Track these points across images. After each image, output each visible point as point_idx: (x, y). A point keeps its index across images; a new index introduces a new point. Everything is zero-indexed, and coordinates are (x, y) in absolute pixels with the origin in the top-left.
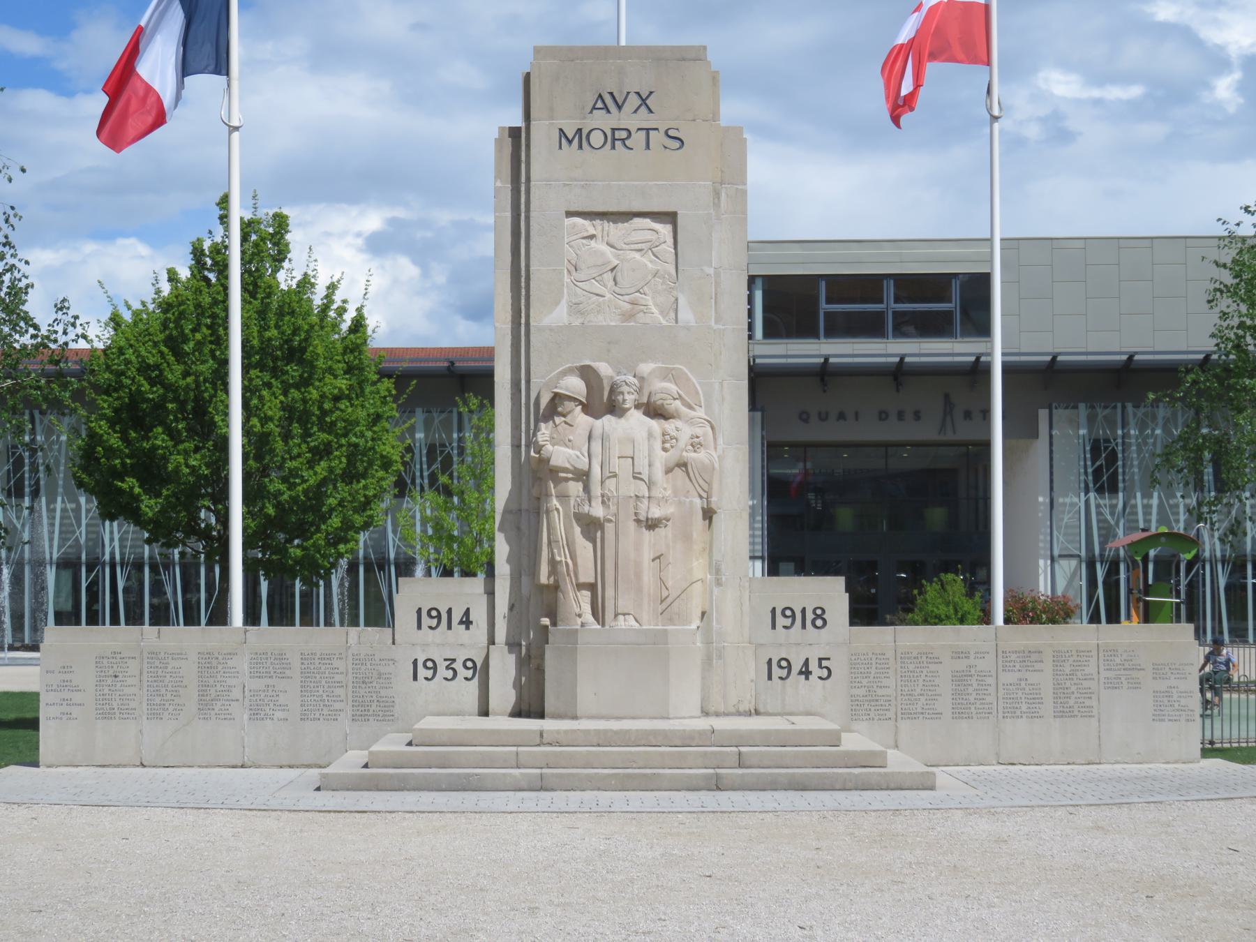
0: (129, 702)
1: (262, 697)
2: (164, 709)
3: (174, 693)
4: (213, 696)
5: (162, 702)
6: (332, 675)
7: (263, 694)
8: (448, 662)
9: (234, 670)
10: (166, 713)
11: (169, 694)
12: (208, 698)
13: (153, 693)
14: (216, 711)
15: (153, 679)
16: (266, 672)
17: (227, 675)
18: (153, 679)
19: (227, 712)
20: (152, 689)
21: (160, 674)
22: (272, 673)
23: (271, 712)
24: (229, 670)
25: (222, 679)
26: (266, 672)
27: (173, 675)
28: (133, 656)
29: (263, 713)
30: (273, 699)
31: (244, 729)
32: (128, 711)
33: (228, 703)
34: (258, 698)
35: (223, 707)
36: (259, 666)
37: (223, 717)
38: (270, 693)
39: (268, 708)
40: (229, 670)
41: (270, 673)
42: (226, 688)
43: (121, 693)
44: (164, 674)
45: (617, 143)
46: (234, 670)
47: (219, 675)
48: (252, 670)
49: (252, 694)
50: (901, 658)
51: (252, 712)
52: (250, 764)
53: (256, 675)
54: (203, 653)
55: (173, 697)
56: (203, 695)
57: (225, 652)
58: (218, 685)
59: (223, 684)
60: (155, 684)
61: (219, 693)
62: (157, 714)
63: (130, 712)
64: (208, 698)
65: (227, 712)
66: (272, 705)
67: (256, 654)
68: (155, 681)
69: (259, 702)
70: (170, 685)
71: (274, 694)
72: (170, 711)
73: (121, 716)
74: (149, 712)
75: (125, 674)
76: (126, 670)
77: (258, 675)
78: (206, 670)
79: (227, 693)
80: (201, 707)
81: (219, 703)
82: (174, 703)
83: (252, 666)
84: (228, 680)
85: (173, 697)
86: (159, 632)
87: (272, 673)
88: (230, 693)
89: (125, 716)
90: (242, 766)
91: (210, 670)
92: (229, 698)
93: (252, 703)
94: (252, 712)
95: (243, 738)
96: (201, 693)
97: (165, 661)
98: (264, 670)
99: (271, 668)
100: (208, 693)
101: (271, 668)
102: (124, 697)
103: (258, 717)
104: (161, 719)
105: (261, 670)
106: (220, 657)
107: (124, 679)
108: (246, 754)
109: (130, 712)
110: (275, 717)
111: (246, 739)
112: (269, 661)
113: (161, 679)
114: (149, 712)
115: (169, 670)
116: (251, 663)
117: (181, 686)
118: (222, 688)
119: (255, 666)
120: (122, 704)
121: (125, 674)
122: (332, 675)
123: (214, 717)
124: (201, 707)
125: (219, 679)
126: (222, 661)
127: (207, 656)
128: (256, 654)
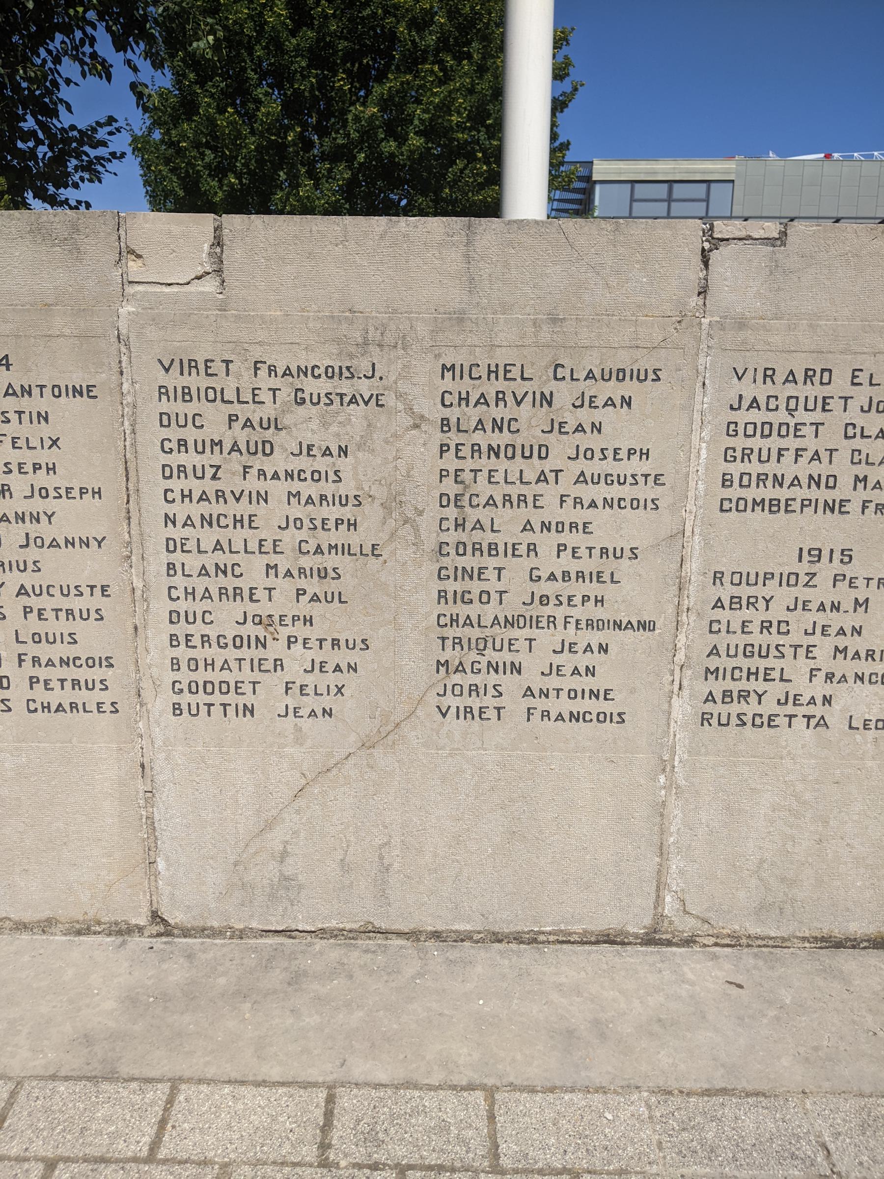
0: (78, 626)
1: (777, 612)
2: (258, 665)
3: (313, 586)
4: (513, 606)
5: (250, 630)
6: (580, 515)
7: (783, 596)
8: (545, 529)
9: (636, 466)
10: (273, 682)
11: (285, 587)
12: (490, 611)
13: (200, 584)
14: (532, 677)
15: (196, 510)
16: (815, 481)
17: (600, 492)
18: (196, 510)
19: (586, 683)
20: (193, 563)
21: (230, 482)
22: (845, 481)
23: (819, 688)
24: (609, 466)
25: (570, 514)
26: (815, 481)
27: (309, 489)
28: (78, 379)
29: (776, 690)
30: (835, 620)
31: (666, 766)
32: (70, 673)
33: (595, 638)
34: (757, 616)
35: (563, 659)
36: (775, 443)
37: (565, 705)
38: (823, 592)
39: (804, 665)
40: (609, 466)
41: (832, 483)
42: (588, 565)
43: (28, 580)
44: (253, 484)
45: (741, 699)
46: (636, 466)
47: (550, 493)
48: (735, 469)
49: (726, 592)
50: (171, 520)
51: (718, 687)
52: (686, 926)
53: (752, 493)
54: (470, 372)
55: (304, 607)
56: (464, 598)
57: (592, 362)
58: (547, 542)
59: (571, 539)
60: (209, 537)
61: (546, 588)
62: (224, 687)
63: (83, 674)
64: (490, 611)
65: (586, 683)
66: (824, 647)
67: (769, 375)
68: (207, 521)
69: (758, 638)
70: (290, 538)
71: (845, 595)
72: (294, 670)
73: (40, 694)
74: (185, 676)
75: (42, 479)
76: (44, 456)
77: (769, 492)
78: (485, 463)
79: (592, 589)
80: (451, 655)
81: (547, 639)
82: (313, 633)
83: (740, 443)
84: (600, 517)
85: (304, 607)
86: (218, 242)
87: (845, 481)
88: (607, 591)
89: (55, 697)
90: (650, 939)
91: (502, 464)
92: (599, 613)
93: (722, 641)
94: (718, 687)
95: (661, 810)
96: (451, 586)
97: (257, 414)
98: (804, 468)
99: (843, 457)
100: (493, 586)
101: (843, 457)
102: (45, 602)
103: (750, 708)
104: (249, 710)
105: (788, 468)
106: (564, 394)
107: (38, 505)
108: (674, 882)
109: (83, 674)
110: (835, 716)
111: (676, 812)
112: (837, 418)
113: (243, 508)
114: (185, 676)
115: (279, 462)
116: (731, 430)
117: (347, 550)
118: (566, 562)
119: (756, 443)
120: (37, 638)
121: (42, 479)
122: (580, 515)
123: (515, 704)
124: (451, 655)
125: (552, 512)
126: (572, 419)
127: (491, 389)
128: (769, 375)
